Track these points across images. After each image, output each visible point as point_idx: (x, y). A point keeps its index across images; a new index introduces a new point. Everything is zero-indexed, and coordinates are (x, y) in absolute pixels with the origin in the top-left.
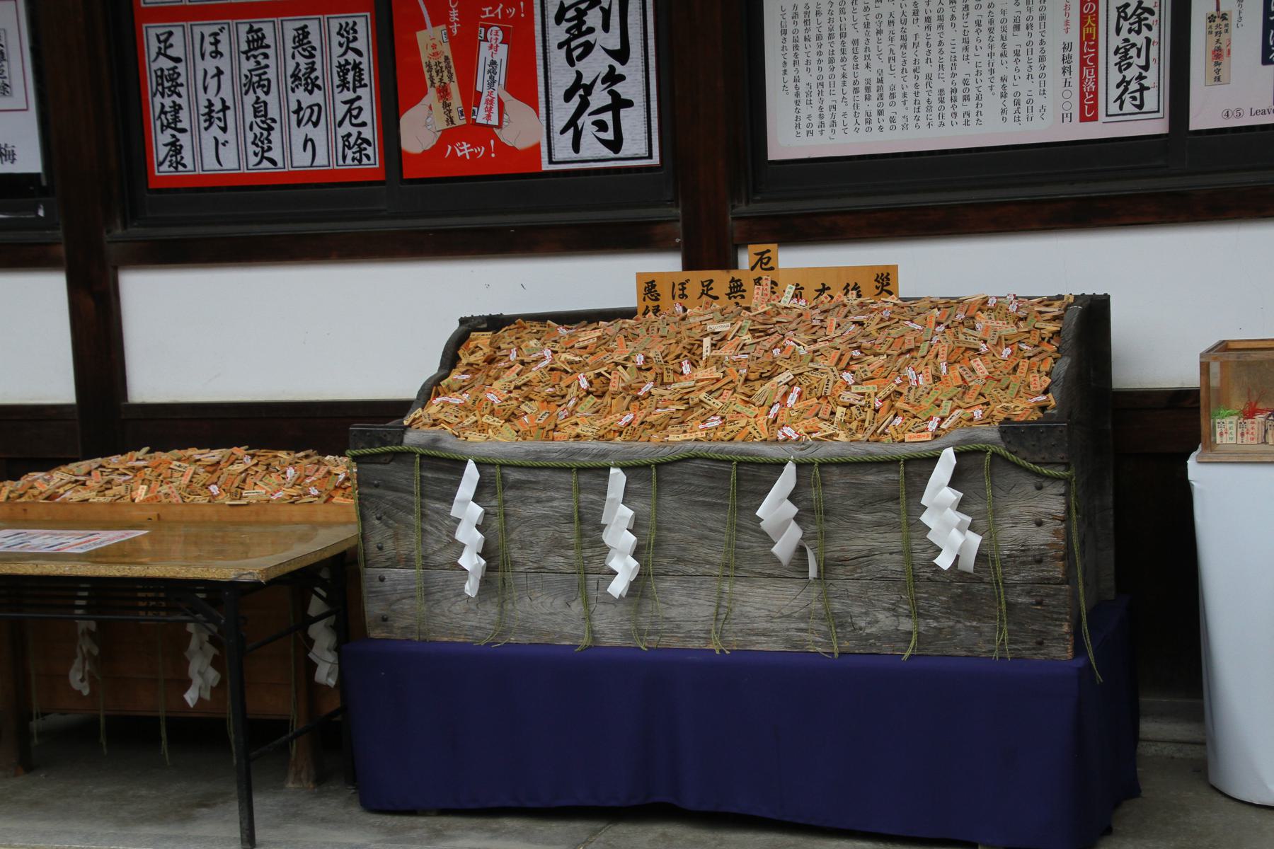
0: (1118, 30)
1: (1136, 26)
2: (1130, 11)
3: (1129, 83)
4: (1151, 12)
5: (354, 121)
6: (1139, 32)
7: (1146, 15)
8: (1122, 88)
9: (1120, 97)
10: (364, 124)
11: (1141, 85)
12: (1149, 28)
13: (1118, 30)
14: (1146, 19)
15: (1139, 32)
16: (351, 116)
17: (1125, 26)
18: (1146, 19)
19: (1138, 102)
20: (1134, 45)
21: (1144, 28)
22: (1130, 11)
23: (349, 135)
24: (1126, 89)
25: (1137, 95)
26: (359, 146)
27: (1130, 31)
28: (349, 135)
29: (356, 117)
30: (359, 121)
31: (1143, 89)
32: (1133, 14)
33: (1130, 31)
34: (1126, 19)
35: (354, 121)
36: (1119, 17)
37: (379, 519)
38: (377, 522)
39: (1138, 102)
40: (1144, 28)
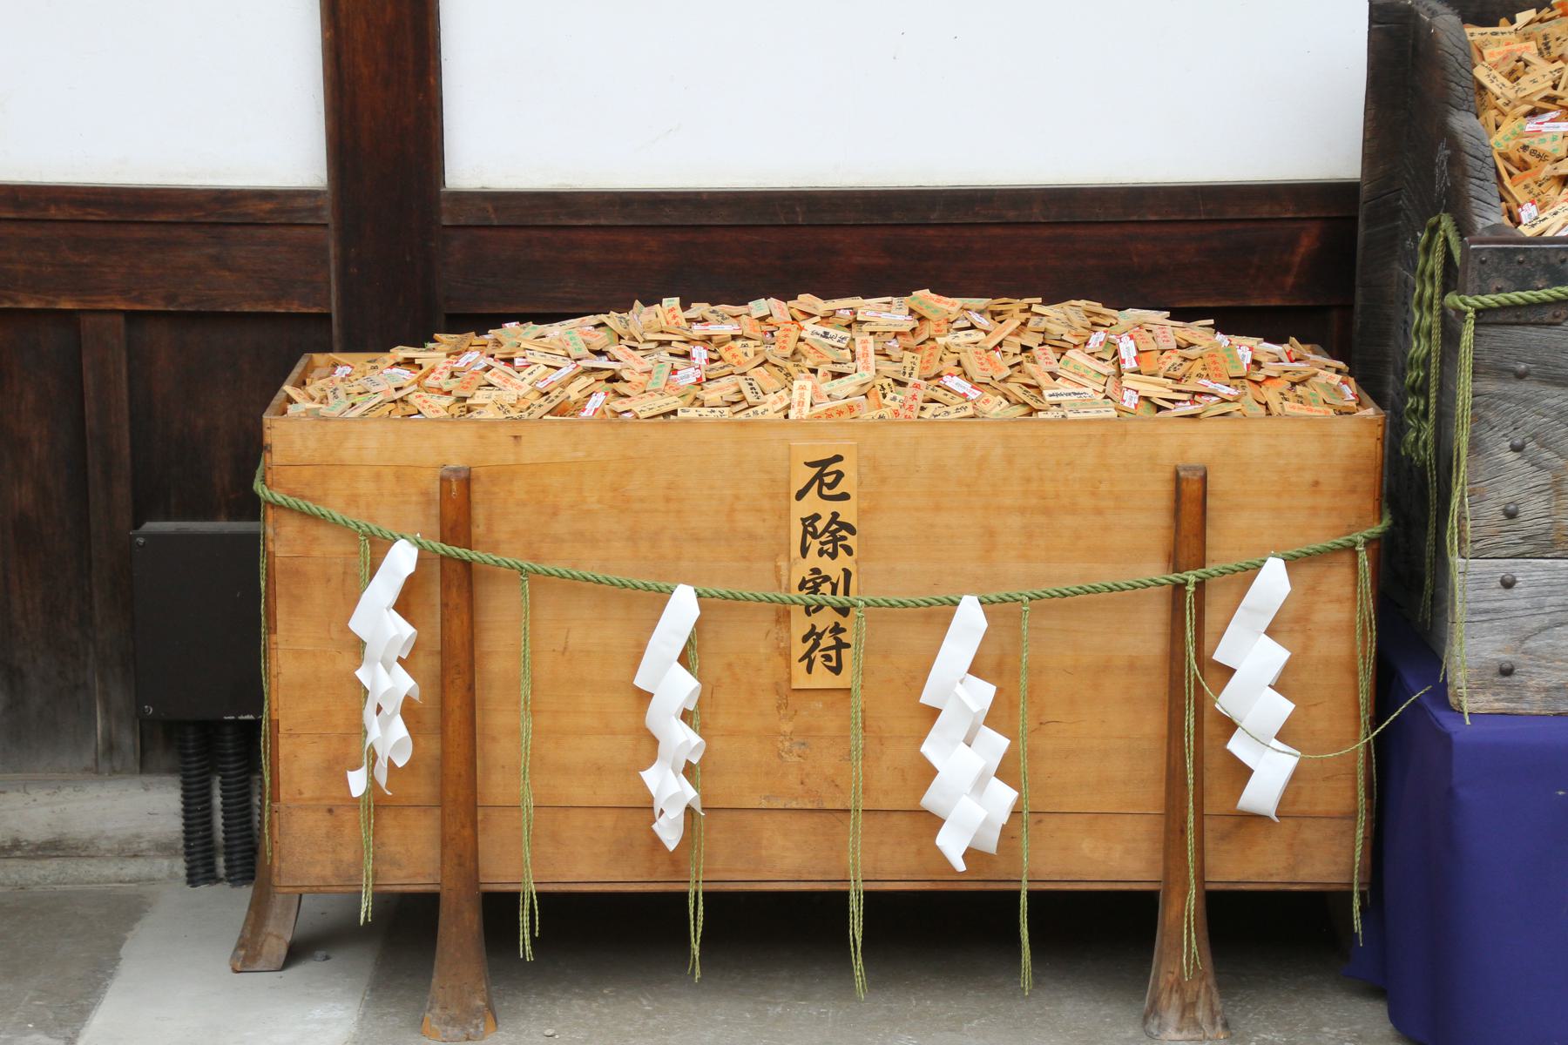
0: (804, 550)
1: (829, 547)
2: (820, 525)
3: (820, 636)
4: (852, 530)
5: (826, 491)
6: (833, 555)
7: (843, 533)
8: (811, 642)
9: (807, 655)
10: (844, 497)
11: (838, 640)
12: (849, 551)
13: (804, 550)
14: (844, 538)
15: (833, 555)
16: (822, 484)
17: (815, 545)
18: (844, 538)
19: (833, 664)
20: (827, 579)
21: (840, 550)
22: (820, 525)
23: (816, 517)
24: (816, 645)
25: (833, 653)
26: (833, 533)
27: (821, 553)
28: (816, 517)
29: (831, 486)
30: (836, 491)
31: (840, 646)
32: (826, 530)
33: (821, 553)
34: (815, 536)
35: (826, 491)
36: (805, 532)
37: (1515, 449)
38: (1512, 456)
39: (833, 664)
40: (840, 550)
